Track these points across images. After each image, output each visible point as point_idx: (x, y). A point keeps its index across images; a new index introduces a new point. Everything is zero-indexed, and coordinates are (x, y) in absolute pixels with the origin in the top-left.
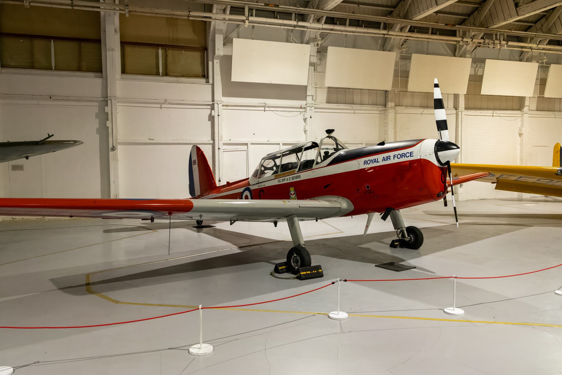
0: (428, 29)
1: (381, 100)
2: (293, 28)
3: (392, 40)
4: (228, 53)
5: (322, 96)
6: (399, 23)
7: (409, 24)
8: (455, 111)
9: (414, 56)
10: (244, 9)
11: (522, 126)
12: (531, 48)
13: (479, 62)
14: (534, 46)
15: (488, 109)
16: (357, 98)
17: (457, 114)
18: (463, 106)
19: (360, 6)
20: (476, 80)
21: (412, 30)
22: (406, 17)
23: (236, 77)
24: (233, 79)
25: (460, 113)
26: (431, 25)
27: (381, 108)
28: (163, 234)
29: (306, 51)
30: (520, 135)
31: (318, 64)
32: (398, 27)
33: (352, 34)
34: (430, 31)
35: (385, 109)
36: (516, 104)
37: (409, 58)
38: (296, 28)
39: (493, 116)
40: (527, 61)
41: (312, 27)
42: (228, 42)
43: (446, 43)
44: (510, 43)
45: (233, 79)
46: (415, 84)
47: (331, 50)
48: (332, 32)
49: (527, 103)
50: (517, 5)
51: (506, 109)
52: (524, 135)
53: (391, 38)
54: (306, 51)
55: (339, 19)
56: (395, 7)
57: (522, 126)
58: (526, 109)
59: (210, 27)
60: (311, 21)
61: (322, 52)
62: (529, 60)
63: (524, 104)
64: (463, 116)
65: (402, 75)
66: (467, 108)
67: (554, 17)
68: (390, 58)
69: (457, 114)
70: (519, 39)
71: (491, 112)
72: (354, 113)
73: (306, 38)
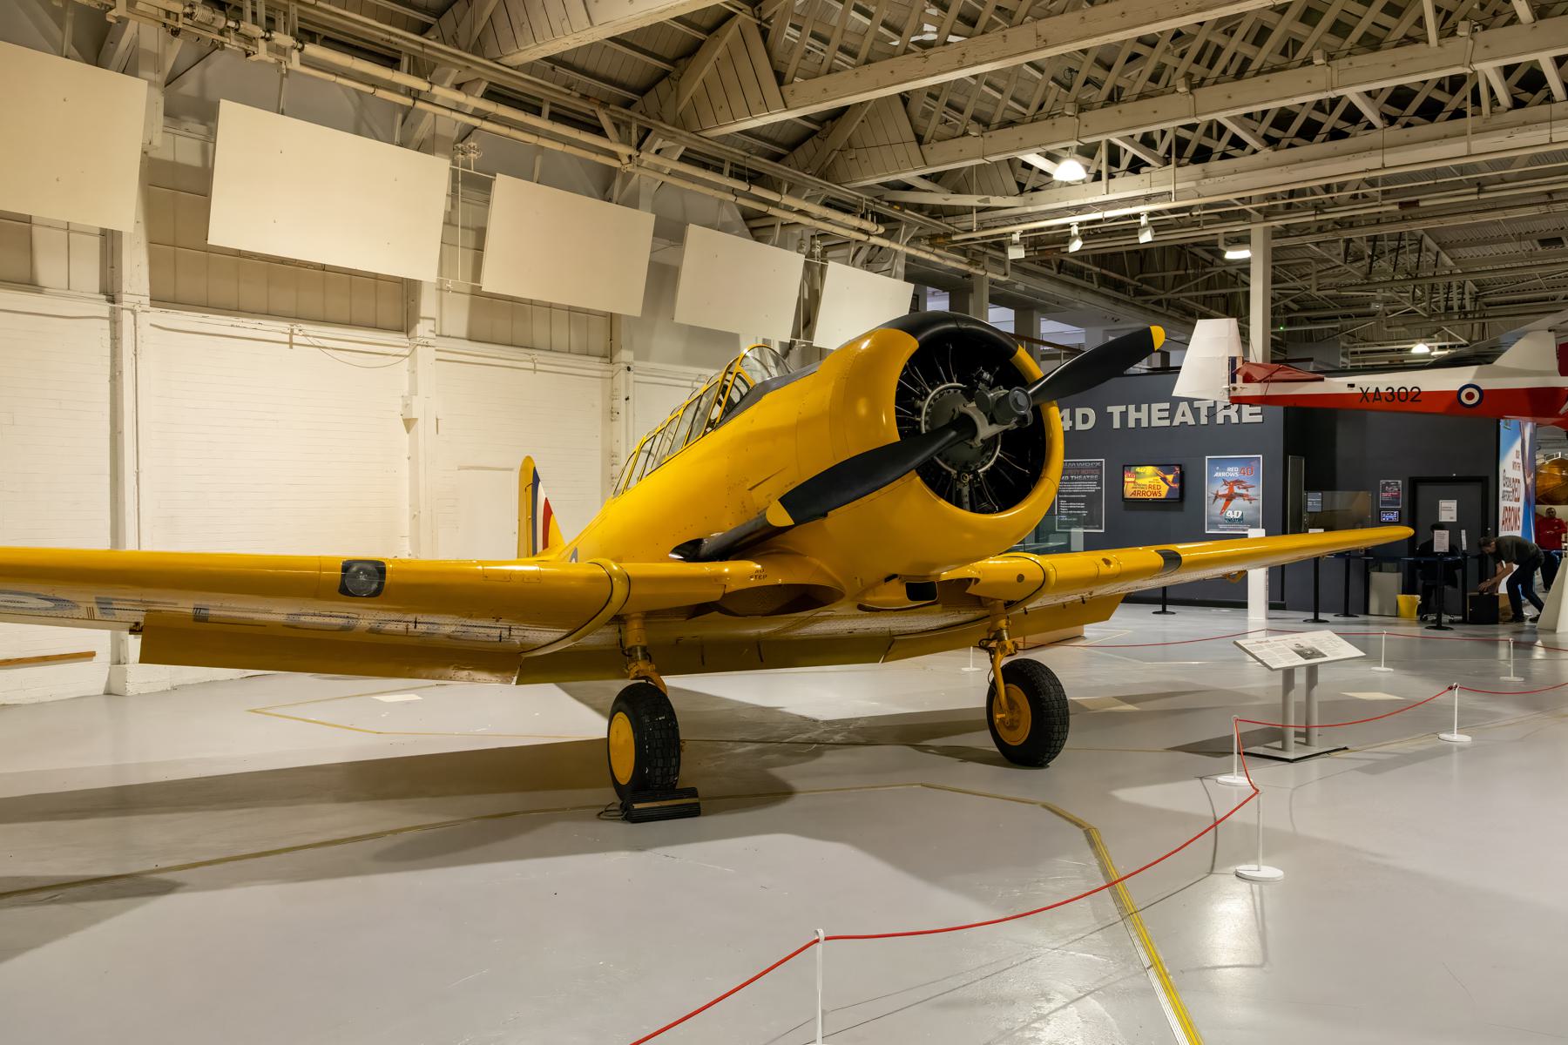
1: (599, 341)
2: (408, 101)
3: (429, 116)
5: (458, 319)
7: (484, 70)
8: (104, 309)
11: (414, 392)
12: (414, 94)
13: (191, 111)
14: (443, 93)
15: (269, 314)
16: (540, 332)
17: (115, 322)
18: (145, 288)
20: (176, 191)
22: (478, 48)
25: (127, 317)
26: (550, 90)
27: (595, 365)
28: (1060, 601)
29: (431, 175)
30: (409, 423)
31: (467, 232)
32: (454, 75)
34: (546, 109)
35: (610, 367)
36: (386, 305)
37: (486, 186)
38: (381, 93)
39: (291, 344)
40: (421, 147)
41: (658, 165)
43: (582, 160)
44: (312, 50)
46: (690, 306)
47: (503, 185)
48: (487, 125)
49: (428, 304)
50: (780, 78)
51: (350, 324)
52: (420, 423)
53: (423, 113)
54: (431, 175)
57: (414, 392)
58: (423, 329)
59: (116, 43)
60: (448, 84)
63: (417, 307)
64: (144, 328)
65: (662, 280)
66: (158, 300)
67: (850, 128)
69: (115, 322)
70: (756, 178)
71: (284, 326)
72: (535, 370)
73: (423, 130)
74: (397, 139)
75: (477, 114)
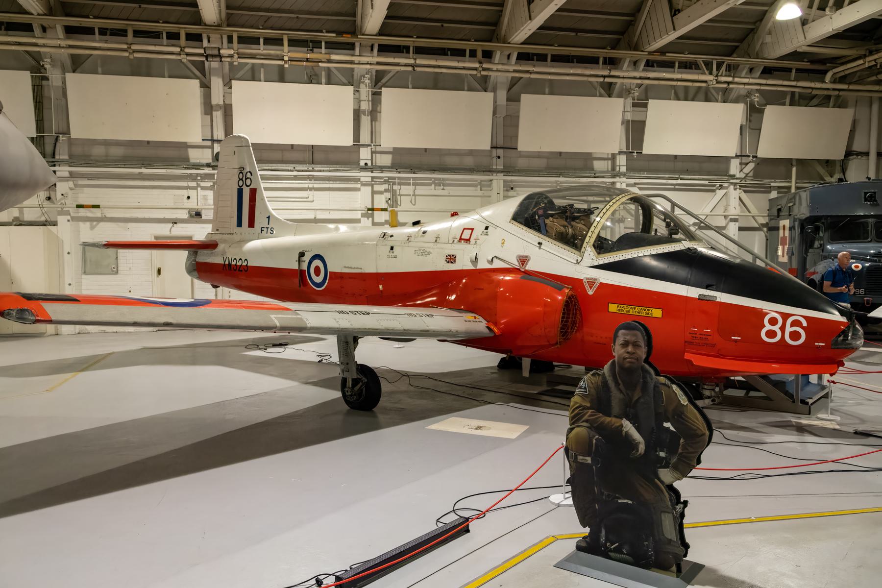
0: (546, 55)
2: (725, 86)
4: (639, 118)
6: (626, 55)
9: (524, 97)
10: (282, 40)
19: (579, 34)
21: (649, 64)
23: (650, 147)
24: (645, 151)
29: (734, 114)
31: (366, 115)
33: (742, 86)
41: (744, 82)
42: (228, 85)
45: (645, 151)
47: (384, 91)
55: (537, 55)
56: (623, 33)
61: (755, 113)
62: (736, 101)
68: (482, 104)
73: (733, 95)
74: (466, 88)
75: (515, 71)
